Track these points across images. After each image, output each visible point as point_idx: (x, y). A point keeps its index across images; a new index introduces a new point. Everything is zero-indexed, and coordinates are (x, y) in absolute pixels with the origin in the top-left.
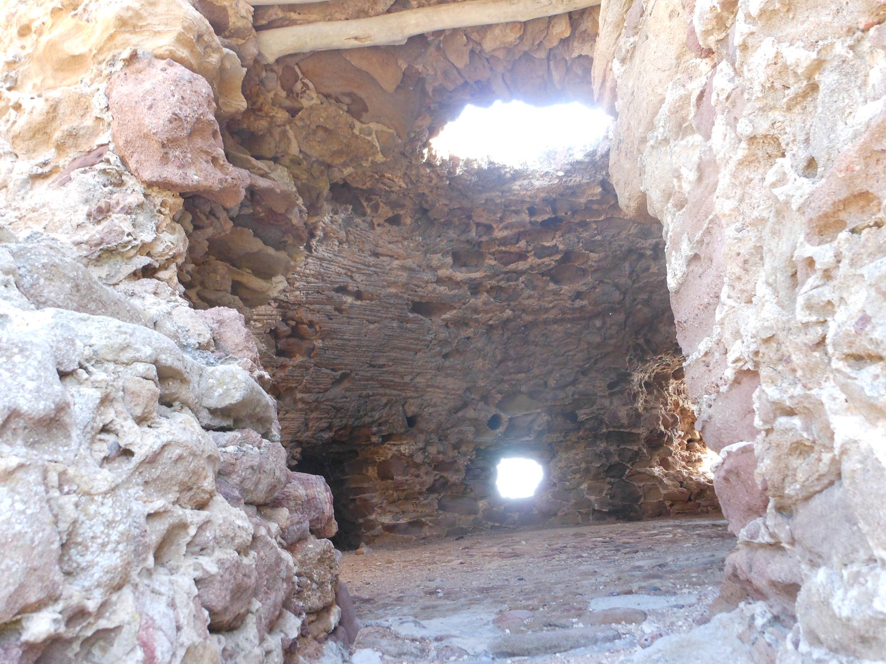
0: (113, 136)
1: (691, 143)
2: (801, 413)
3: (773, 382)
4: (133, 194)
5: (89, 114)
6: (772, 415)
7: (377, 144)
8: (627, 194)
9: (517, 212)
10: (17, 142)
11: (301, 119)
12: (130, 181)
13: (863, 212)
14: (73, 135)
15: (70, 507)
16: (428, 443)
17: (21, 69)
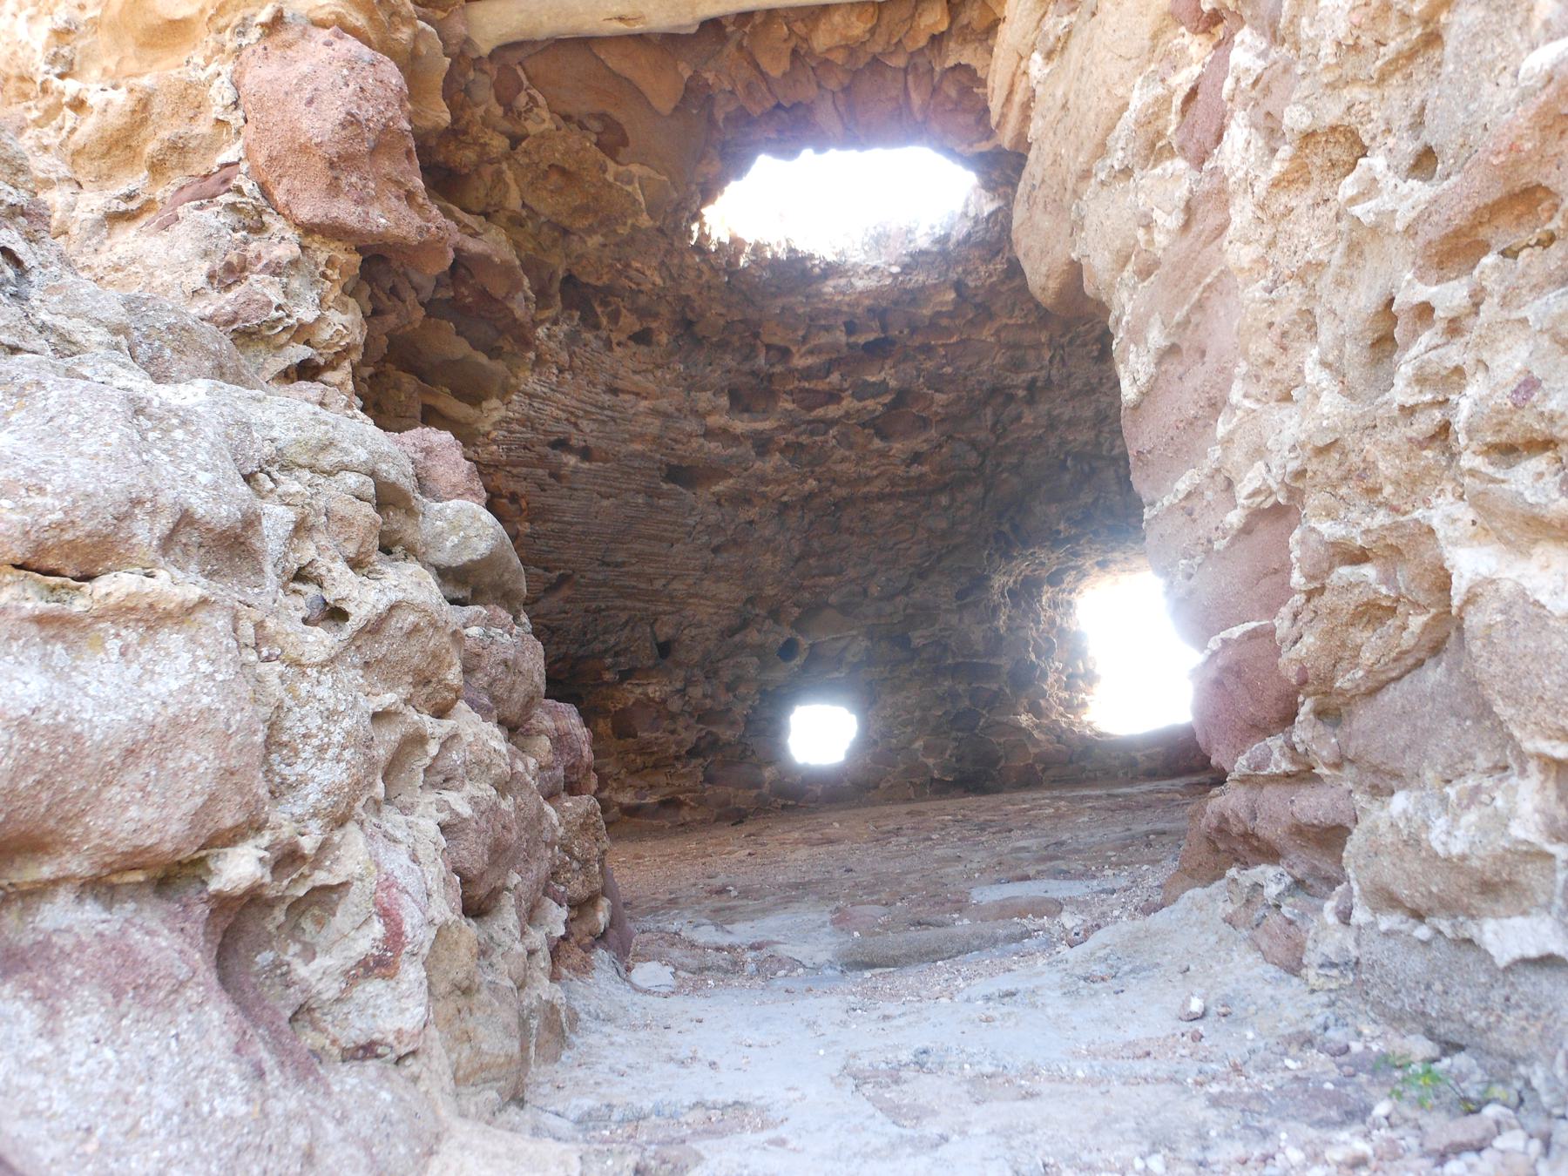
0: (247, 149)
1: (1170, 171)
2: (1377, 556)
3: (1328, 515)
4: (281, 244)
5: (202, 117)
6: (1325, 566)
7: (641, 199)
8: (1044, 269)
9: (827, 329)
10: (80, 161)
11: (526, 152)
12: (276, 224)
13: (1518, 225)
14: (178, 148)
15: (273, 680)
16: (689, 682)
17: (80, 44)
